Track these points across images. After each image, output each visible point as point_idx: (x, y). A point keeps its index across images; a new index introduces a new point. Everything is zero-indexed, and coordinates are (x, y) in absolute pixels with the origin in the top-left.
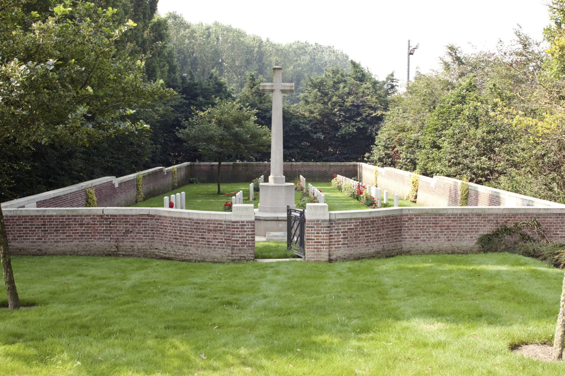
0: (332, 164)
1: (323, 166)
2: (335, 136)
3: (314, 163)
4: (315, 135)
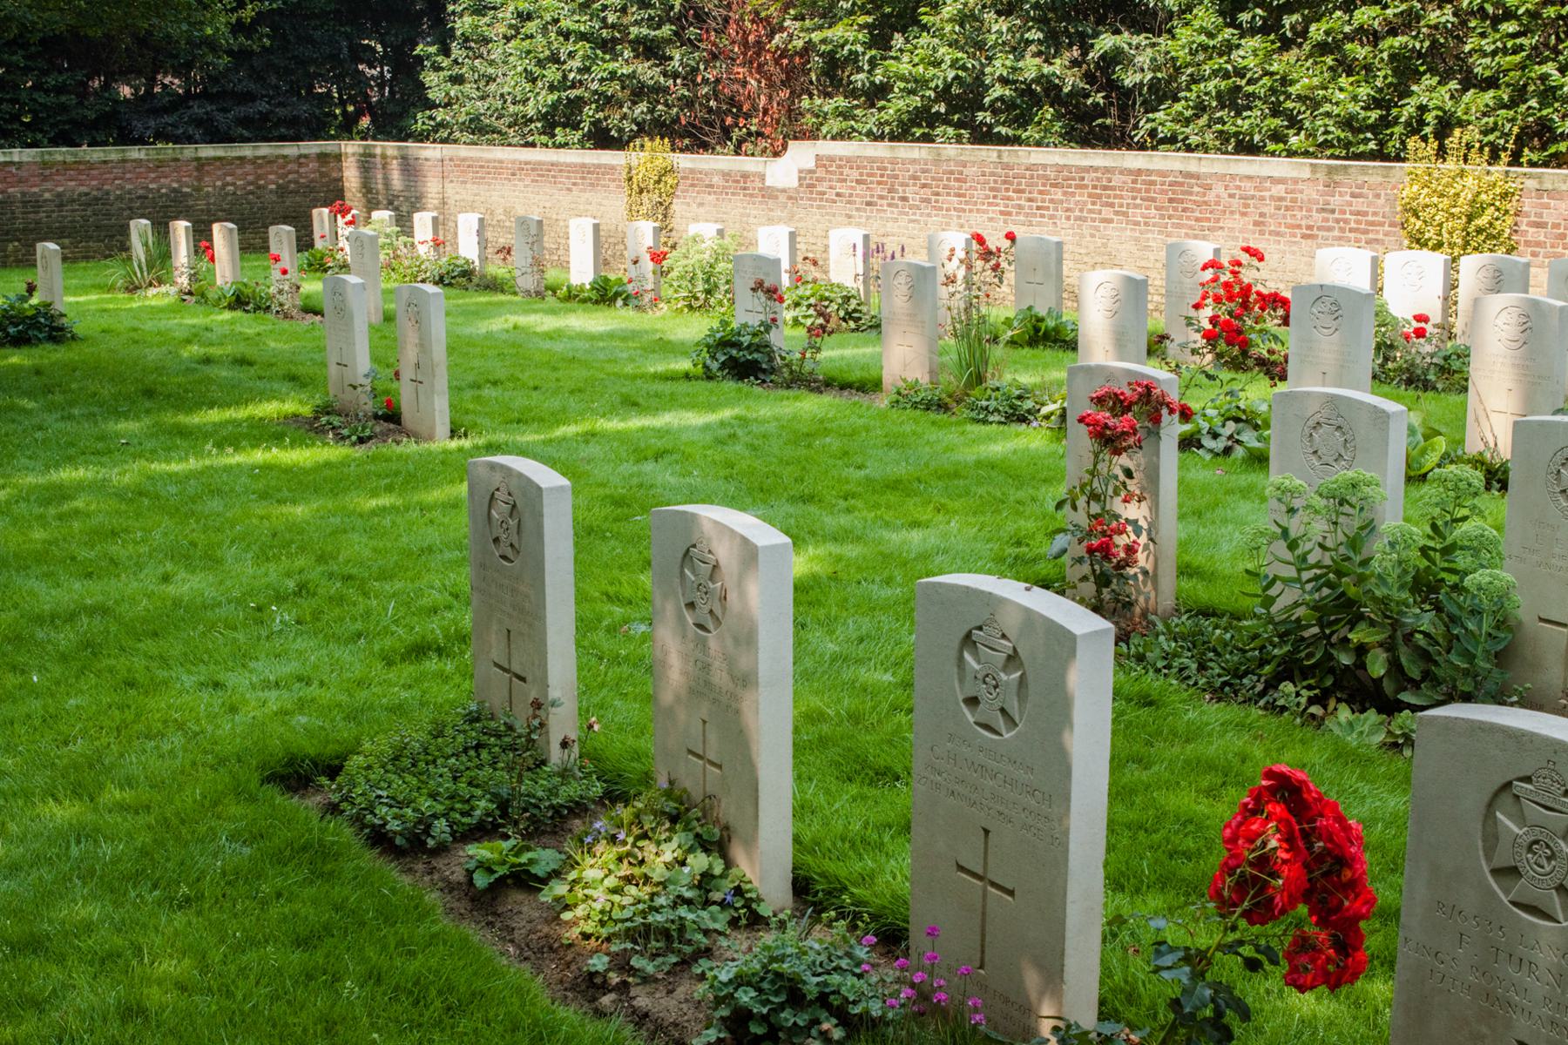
1: (160, 164)
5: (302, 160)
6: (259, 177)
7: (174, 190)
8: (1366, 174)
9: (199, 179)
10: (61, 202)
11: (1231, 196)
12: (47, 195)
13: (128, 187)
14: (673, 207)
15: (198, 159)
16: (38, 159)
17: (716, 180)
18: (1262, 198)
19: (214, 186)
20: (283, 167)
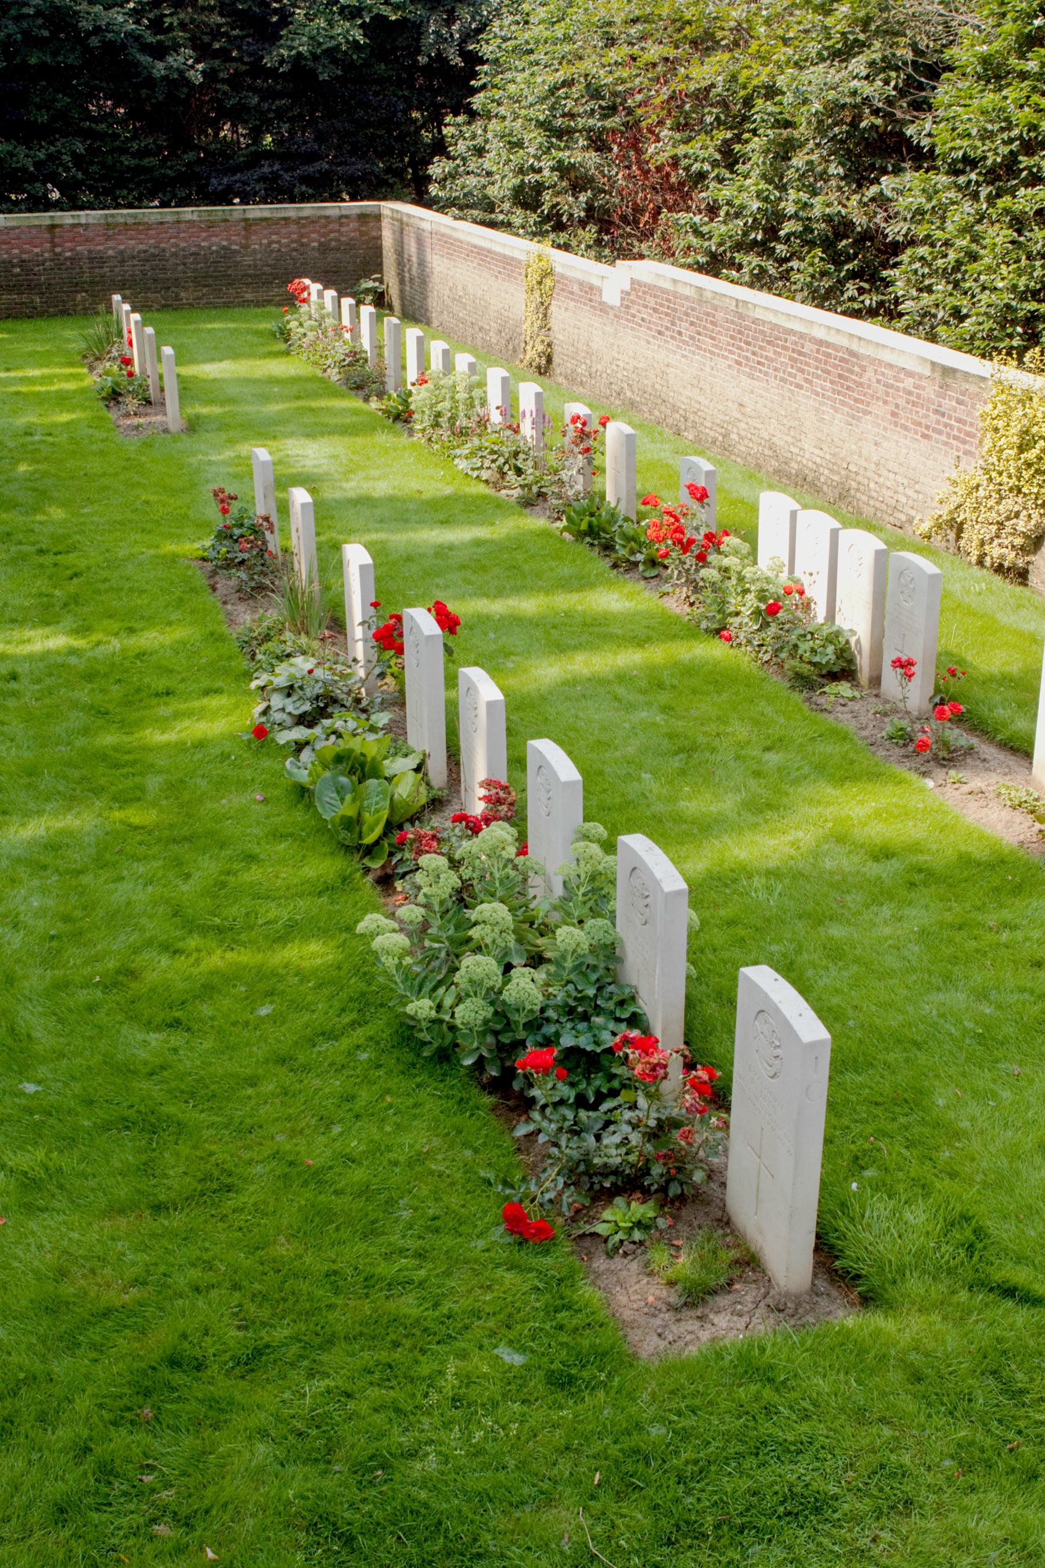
0: (257, 211)
1: (211, 225)
2: (257, 69)
3: (169, 214)
4: (160, 65)
5: (343, 220)
6: (302, 236)
7: (224, 248)
8: (967, 381)
9: (246, 238)
10: (122, 259)
11: (878, 381)
12: (111, 253)
13: (183, 244)
14: (552, 308)
15: (246, 220)
16: (103, 221)
17: (576, 288)
18: (898, 389)
19: (261, 244)
20: (325, 226)
